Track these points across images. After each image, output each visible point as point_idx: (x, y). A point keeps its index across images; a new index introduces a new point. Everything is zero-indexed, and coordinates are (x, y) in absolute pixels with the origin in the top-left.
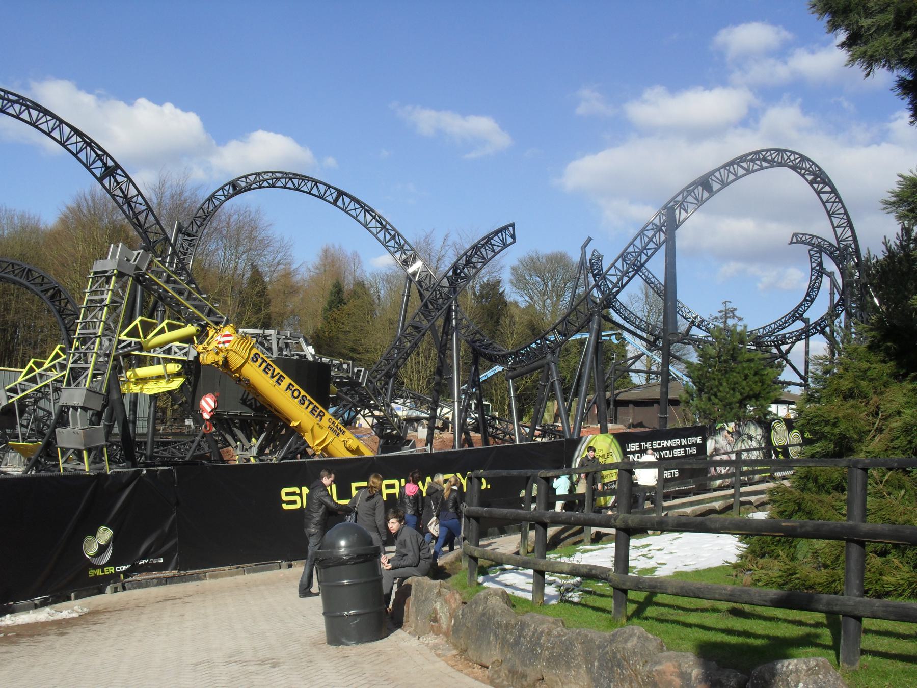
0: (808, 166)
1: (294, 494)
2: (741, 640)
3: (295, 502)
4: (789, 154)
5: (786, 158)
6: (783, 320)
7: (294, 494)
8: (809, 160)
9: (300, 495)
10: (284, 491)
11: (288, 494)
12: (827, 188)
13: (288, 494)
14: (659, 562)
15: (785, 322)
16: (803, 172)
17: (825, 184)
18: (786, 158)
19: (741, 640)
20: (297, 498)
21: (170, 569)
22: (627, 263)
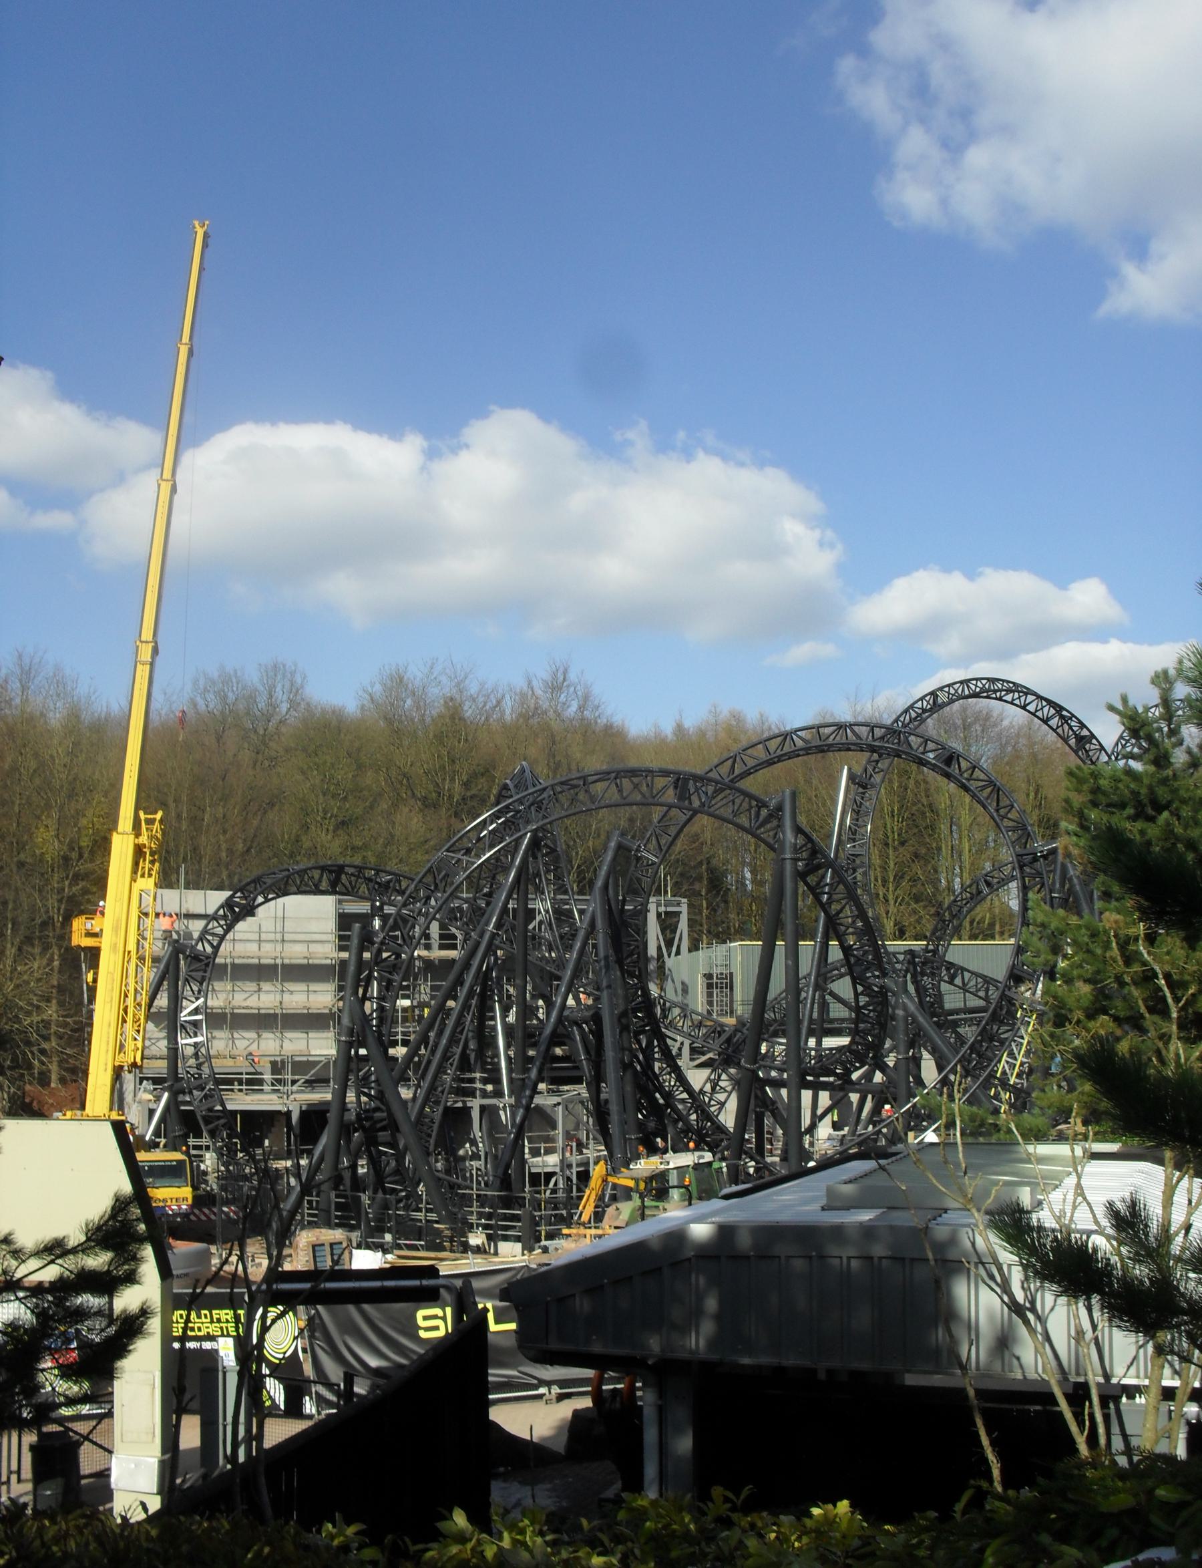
0: (1000, 686)
1: (435, 1317)
2: (816, 1006)
3: (437, 1328)
4: (974, 682)
5: (973, 687)
6: (1009, 698)
7: (435, 1317)
8: (998, 680)
9: (444, 1318)
10: (420, 1314)
11: (425, 1318)
12: (1030, 698)
13: (425, 1318)
14: (967, 1213)
15: (1009, 691)
16: (998, 694)
17: (1026, 694)
18: (973, 687)
19: (816, 1006)
20: (440, 1323)
21: (1058, 1409)
22: (999, 1029)
